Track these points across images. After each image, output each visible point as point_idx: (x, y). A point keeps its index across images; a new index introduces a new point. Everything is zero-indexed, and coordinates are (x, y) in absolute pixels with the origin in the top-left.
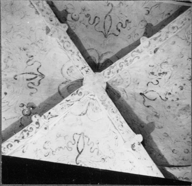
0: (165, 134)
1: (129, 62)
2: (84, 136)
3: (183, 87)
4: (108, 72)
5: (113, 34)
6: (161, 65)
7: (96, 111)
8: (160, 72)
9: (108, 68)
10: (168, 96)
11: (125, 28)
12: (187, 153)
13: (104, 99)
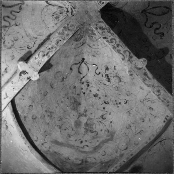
0: (46, 92)
1: (118, 48)
2: (20, 5)
3: (97, 96)
4: (102, 27)
5: (147, 19)
6: (117, 76)
7: (54, 17)
8: (109, 75)
9: (107, 26)
10: (85, 84)
11: (155, 33)
12: (33, 118)
13: (70, 28)
